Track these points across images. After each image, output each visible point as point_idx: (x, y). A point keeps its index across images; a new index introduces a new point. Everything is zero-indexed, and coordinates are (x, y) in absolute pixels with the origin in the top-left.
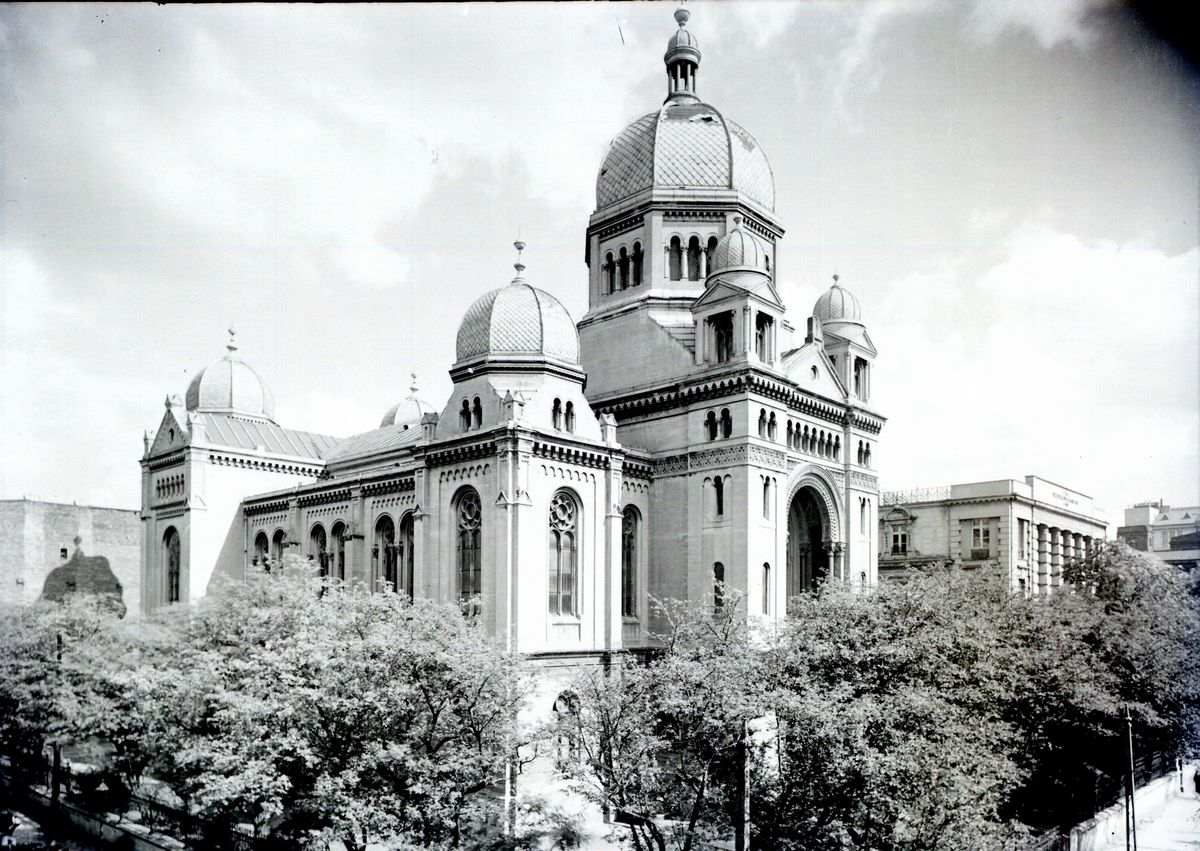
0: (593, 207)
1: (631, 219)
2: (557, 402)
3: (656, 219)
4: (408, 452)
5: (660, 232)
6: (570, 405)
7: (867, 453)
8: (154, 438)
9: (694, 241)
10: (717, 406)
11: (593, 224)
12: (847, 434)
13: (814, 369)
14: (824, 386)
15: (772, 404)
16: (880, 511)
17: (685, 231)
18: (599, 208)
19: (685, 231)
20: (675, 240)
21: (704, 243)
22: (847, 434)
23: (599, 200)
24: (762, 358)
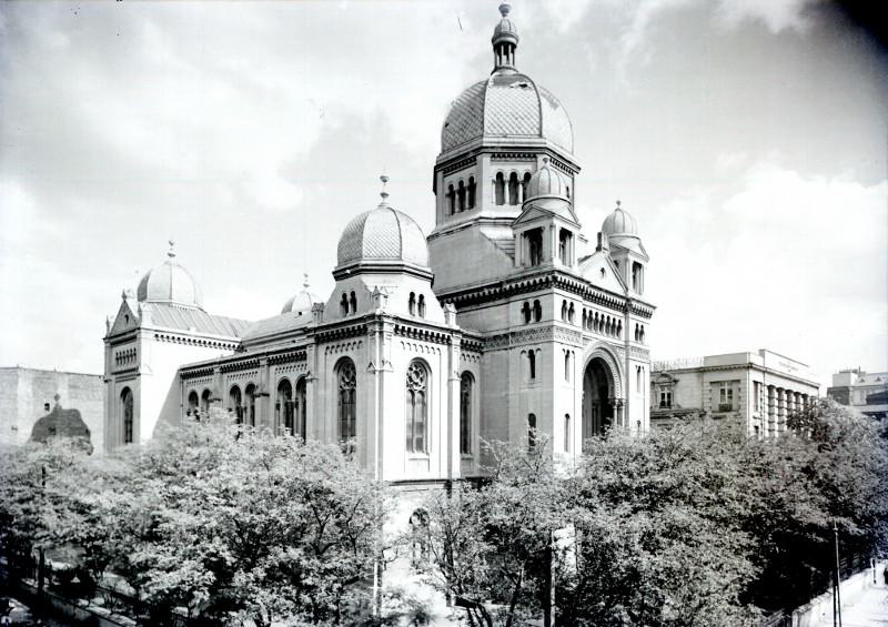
2: (412, 295)
6: (421, 297)
7: (642, 333)
13: (603, 270)
14: (610, 283)
15: (570, 296)
17: (507, 168)
19: (507, 168)
20: (500, 175)
24: (564, 263)
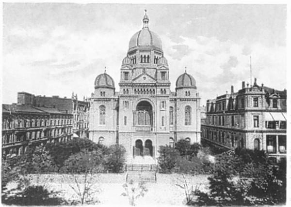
0: (128, 48)
1: (134, 52)
3: (138, 52)
4: (256, 122)
5: (138, 54)
8: (138, 82)
9: (145, 56)
10: (163, 88)
11: (131, 50)
12: (157, 89)
16: (202, 122)
17: (143, 54)
18: (129, 49)
19: (143, 54)
20: (141, 56)
21: (147, 56)
22: (157, 89)
23: (129, 47)
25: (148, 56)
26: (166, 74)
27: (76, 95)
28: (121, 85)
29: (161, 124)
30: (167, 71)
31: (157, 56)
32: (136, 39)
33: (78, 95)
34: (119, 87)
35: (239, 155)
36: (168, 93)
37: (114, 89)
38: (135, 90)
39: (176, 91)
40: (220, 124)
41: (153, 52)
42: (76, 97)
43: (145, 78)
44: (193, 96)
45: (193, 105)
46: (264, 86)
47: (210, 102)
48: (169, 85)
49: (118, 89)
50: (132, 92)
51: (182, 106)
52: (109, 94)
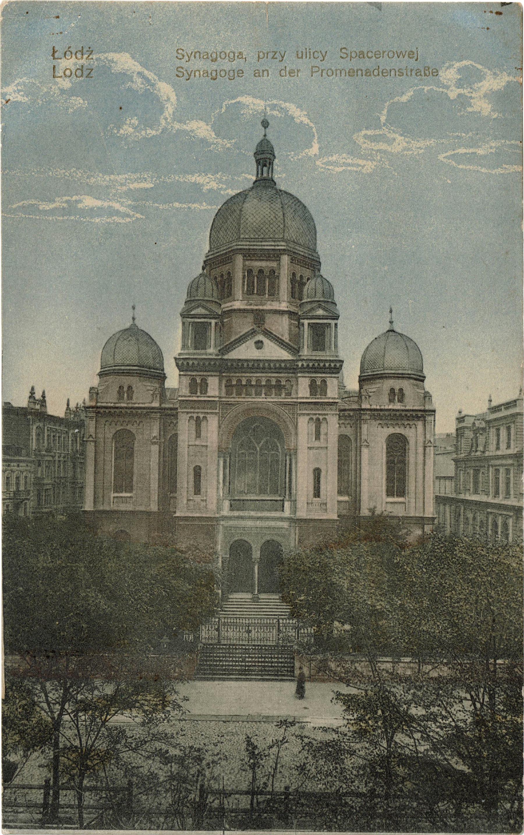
25: (401, 390)
26: (327, 331)
27: (44, 396)
28: (183, 365)
29: (192, 490)
30: (333, 322)
31: (300, 271)
32: (229, 212)
33: (46, 393)
34: (177, 372)
35: (404, 132)
36: (332, 392)
37: (162, 378)
38: (229, 380)
39: (361, 387)
40: (497, 493)
41: (285, 259)
42: (43, 402)
43: (259, 345)
44: (411, 403)
45: (414, 434)
46: (291, 687)
47: (468, 422)
48: (335, 368)
49: (173, 379)
50: (214, 387)
51: (376, 437)
52: (143, 395)
